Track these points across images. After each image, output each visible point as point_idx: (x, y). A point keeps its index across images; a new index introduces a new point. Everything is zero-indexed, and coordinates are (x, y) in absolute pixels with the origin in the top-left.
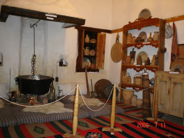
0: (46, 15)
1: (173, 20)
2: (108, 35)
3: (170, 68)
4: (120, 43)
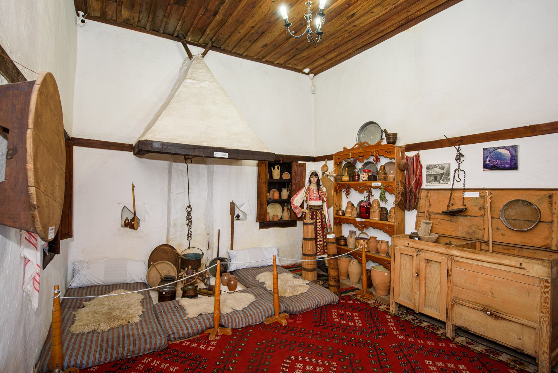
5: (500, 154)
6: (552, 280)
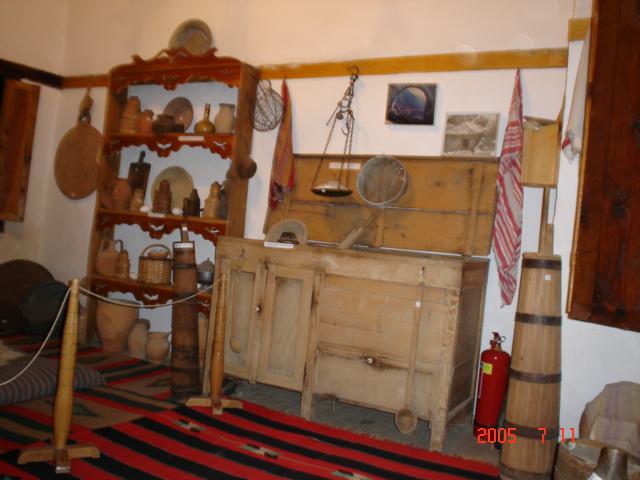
4: (96, 131)
5: (412, 96)
6: (461, 293)
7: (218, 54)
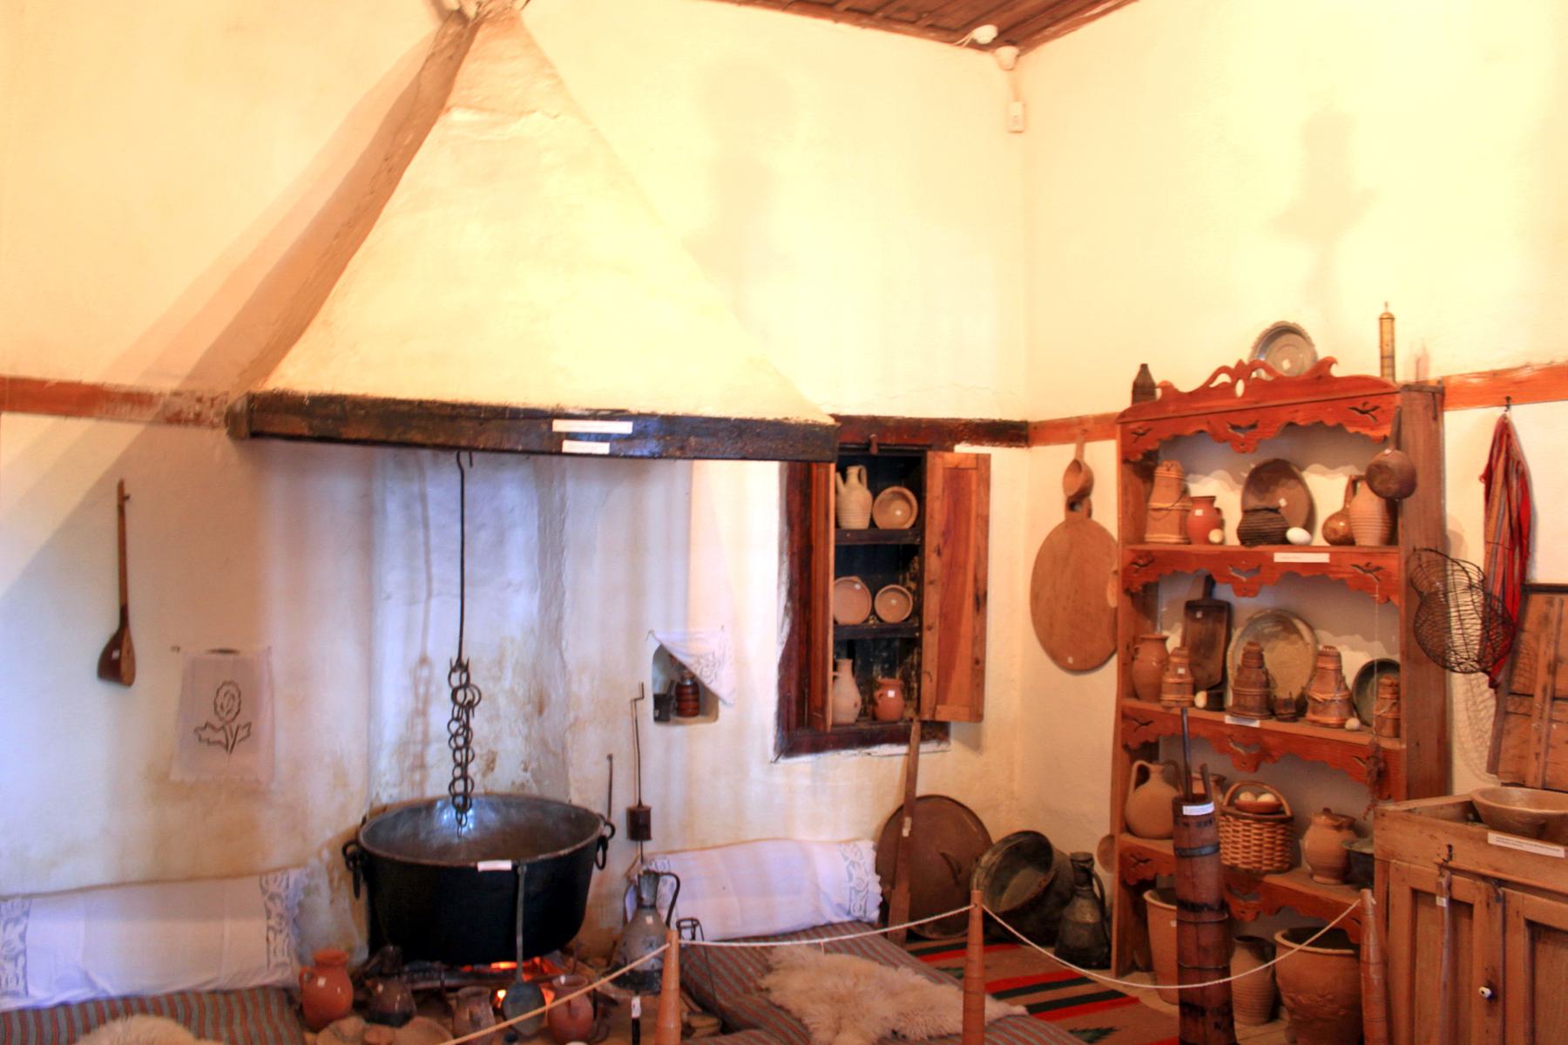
0: (559, 426)
1: (1506, 388)
2: (1002, 458)
3: (1493, 767)
4: (1102, 531)
7: (1336, 371)
